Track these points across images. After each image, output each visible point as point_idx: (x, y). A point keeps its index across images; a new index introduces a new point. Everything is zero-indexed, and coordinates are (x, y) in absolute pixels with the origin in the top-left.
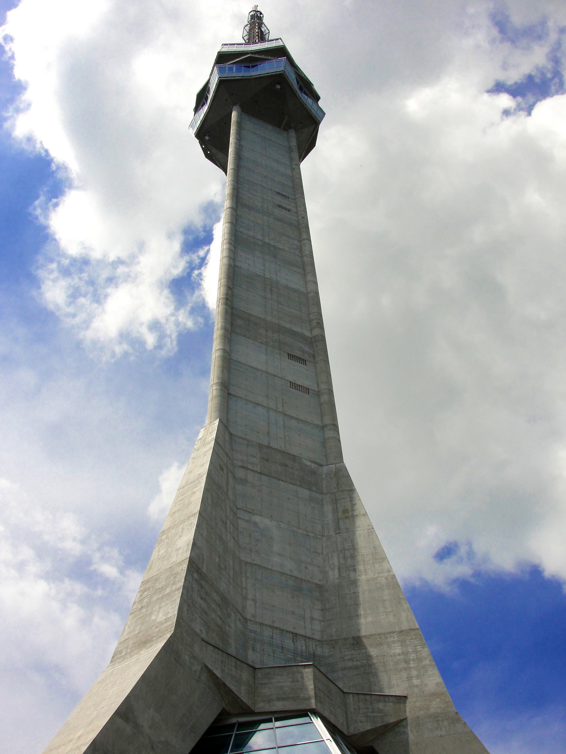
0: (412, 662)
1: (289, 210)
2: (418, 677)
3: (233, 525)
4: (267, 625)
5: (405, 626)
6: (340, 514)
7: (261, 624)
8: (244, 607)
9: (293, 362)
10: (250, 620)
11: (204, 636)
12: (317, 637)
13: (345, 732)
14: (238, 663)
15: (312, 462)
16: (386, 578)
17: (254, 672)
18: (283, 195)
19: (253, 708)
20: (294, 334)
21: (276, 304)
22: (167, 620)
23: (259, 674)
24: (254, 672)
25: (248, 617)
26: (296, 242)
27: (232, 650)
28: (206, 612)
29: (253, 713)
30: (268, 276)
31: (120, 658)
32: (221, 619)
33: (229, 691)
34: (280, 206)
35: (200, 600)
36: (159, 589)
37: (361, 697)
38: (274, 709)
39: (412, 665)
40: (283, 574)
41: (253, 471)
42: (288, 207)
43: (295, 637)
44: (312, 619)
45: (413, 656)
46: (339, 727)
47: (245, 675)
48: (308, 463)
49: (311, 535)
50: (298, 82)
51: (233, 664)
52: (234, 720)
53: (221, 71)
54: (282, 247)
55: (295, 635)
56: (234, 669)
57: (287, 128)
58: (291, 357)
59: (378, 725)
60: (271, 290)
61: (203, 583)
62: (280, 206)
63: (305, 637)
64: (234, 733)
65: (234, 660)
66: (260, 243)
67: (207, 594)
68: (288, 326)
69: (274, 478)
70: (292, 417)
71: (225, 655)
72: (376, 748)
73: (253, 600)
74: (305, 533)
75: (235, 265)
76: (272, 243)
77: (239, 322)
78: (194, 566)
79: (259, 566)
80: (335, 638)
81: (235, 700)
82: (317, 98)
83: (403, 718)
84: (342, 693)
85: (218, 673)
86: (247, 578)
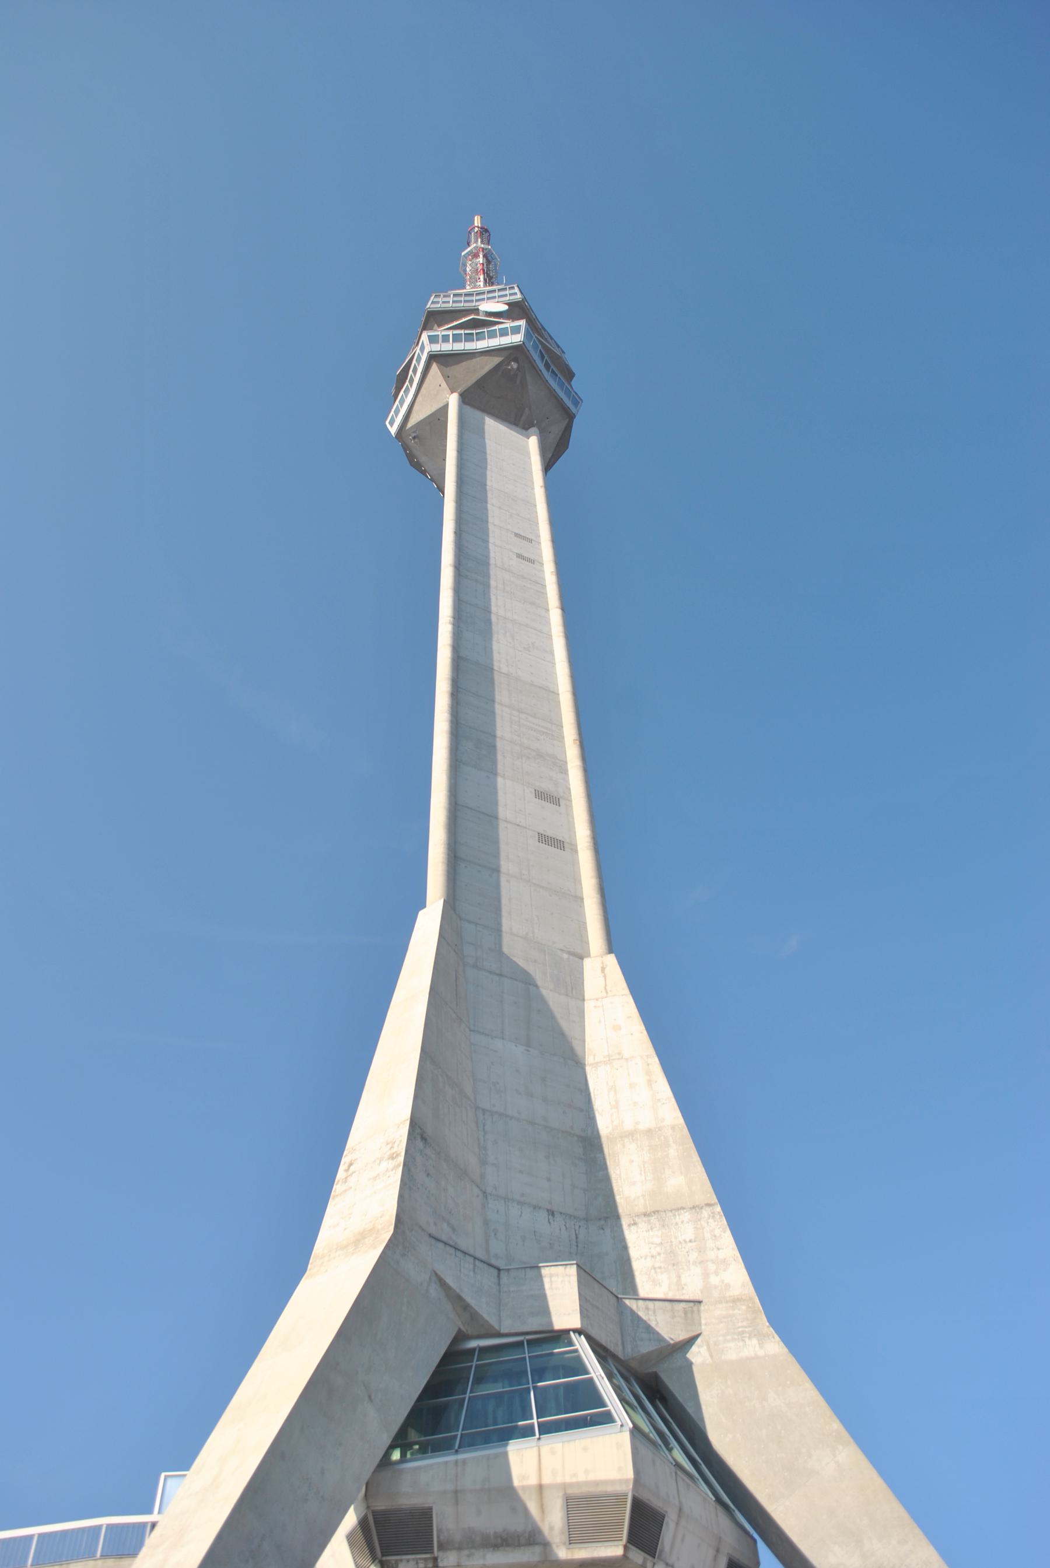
2: (717, 1273)
5: (735, 1292)
8: (482, 1176)
11: (432, 1230)
14: (477, 1262)
17: (499, 1276)
19: (497, 1327)
23: (503, 1274)
24: (499, 1276)
25: (489, 1190)
33: (467, 1307)
46: (612, 1349)
50: (542, 357)
51: (472, 1266)
52: (473, 1344)
56: (472, 1274)
62: (519, 556)
64: (474, 1364)
65: (471, 1259)
70: (486, 1222)
72: (664, 1377)
81: (474, 1316)
82: (569, 375)
83: (695, 1333)
85: (449, 1281)
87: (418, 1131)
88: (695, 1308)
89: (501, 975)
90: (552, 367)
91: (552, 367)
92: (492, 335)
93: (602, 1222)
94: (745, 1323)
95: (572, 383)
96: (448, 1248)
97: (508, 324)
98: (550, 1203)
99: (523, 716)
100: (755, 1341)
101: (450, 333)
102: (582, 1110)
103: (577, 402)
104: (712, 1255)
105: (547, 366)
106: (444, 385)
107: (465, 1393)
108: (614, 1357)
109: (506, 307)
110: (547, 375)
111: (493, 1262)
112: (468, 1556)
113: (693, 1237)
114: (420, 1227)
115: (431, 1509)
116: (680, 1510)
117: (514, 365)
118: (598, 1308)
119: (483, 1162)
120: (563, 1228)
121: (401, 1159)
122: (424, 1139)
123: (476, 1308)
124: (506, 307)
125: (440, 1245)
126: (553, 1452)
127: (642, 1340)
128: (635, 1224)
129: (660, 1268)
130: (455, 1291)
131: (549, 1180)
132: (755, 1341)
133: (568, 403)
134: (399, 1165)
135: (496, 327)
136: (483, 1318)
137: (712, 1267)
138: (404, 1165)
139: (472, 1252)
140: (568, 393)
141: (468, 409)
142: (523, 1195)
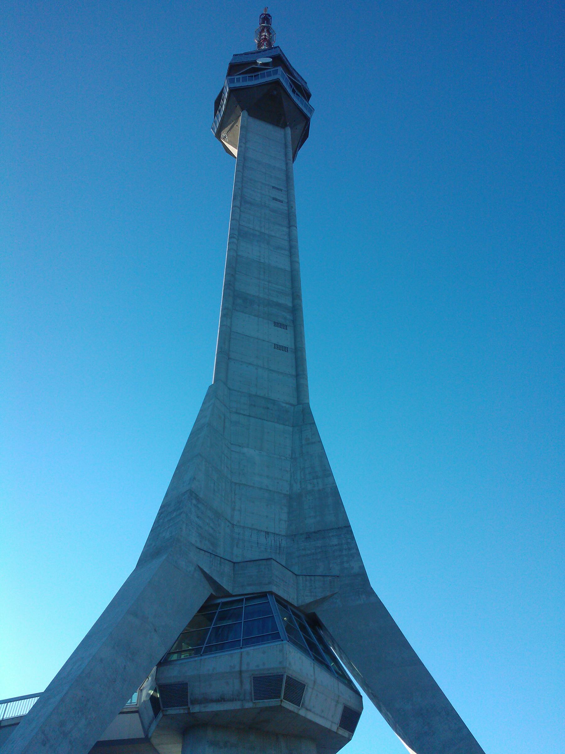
0: (344, 551)
1: (281, 202)
3: (227, 457)
4: (248, 528)
6: (304, 442)
7: (244, 527)
11: (198, 545)
12: (283, 533)
14: (222, 560)
15: (287, 403)
18: (278, 189)
19: (231, 592)
20: (278, 305)
21: (266, 283)
25: (235, 523)
27: (220, 551)
28: (200, 527)
29: (232, 596)
30: (262, 261)
32: (213, 529)
34: (274, 199)
35: (196, 519)
37: (308, 577)
38: (246, 592)
39: (344, 553)
41: (244, 415)
42: (281, 199)
44: (280, 520)
45: (345, 546)
47: (227, 568)
48: (284, 405)
49: (283, 458)
52: (219, 601)
53: (231, 81)
54: (273, 234)
55: (267, 533)
56: (219, 565)
57: (284, 126)
58: (277, 324)
59: (318, 598)
60: (264, 272)
61: (200, 506)
62: (274, 199)
65: (219, 559)
66: (258, 233)
67: (202, 513)
68: (275, 300)
74: (278, 457)
76: (267, 232)
77: (239, 301)
79: (244, 484)
82: (307, 96)
84: (295, 576)
86: (235, 495)
92: (263, 76)
96: (206, 553)
97: (272, 70)
99: (270, 284)
101: (241, 76)
103: (311, 110)
105: (294, 91)
107: (242, 620)
109: (270, 60)
112: (205, 707)
115: (187, 684)
116: (315, 682)
117: (275, 93)
119: (233, 509)
124: (270, 60)
125: (203, 552)
126: (248, 654)
127: (307, 596)
128: (309, 537)
133: (305, 111)
135: (265, 71)
137: (345, 559)
140: (306, 106)
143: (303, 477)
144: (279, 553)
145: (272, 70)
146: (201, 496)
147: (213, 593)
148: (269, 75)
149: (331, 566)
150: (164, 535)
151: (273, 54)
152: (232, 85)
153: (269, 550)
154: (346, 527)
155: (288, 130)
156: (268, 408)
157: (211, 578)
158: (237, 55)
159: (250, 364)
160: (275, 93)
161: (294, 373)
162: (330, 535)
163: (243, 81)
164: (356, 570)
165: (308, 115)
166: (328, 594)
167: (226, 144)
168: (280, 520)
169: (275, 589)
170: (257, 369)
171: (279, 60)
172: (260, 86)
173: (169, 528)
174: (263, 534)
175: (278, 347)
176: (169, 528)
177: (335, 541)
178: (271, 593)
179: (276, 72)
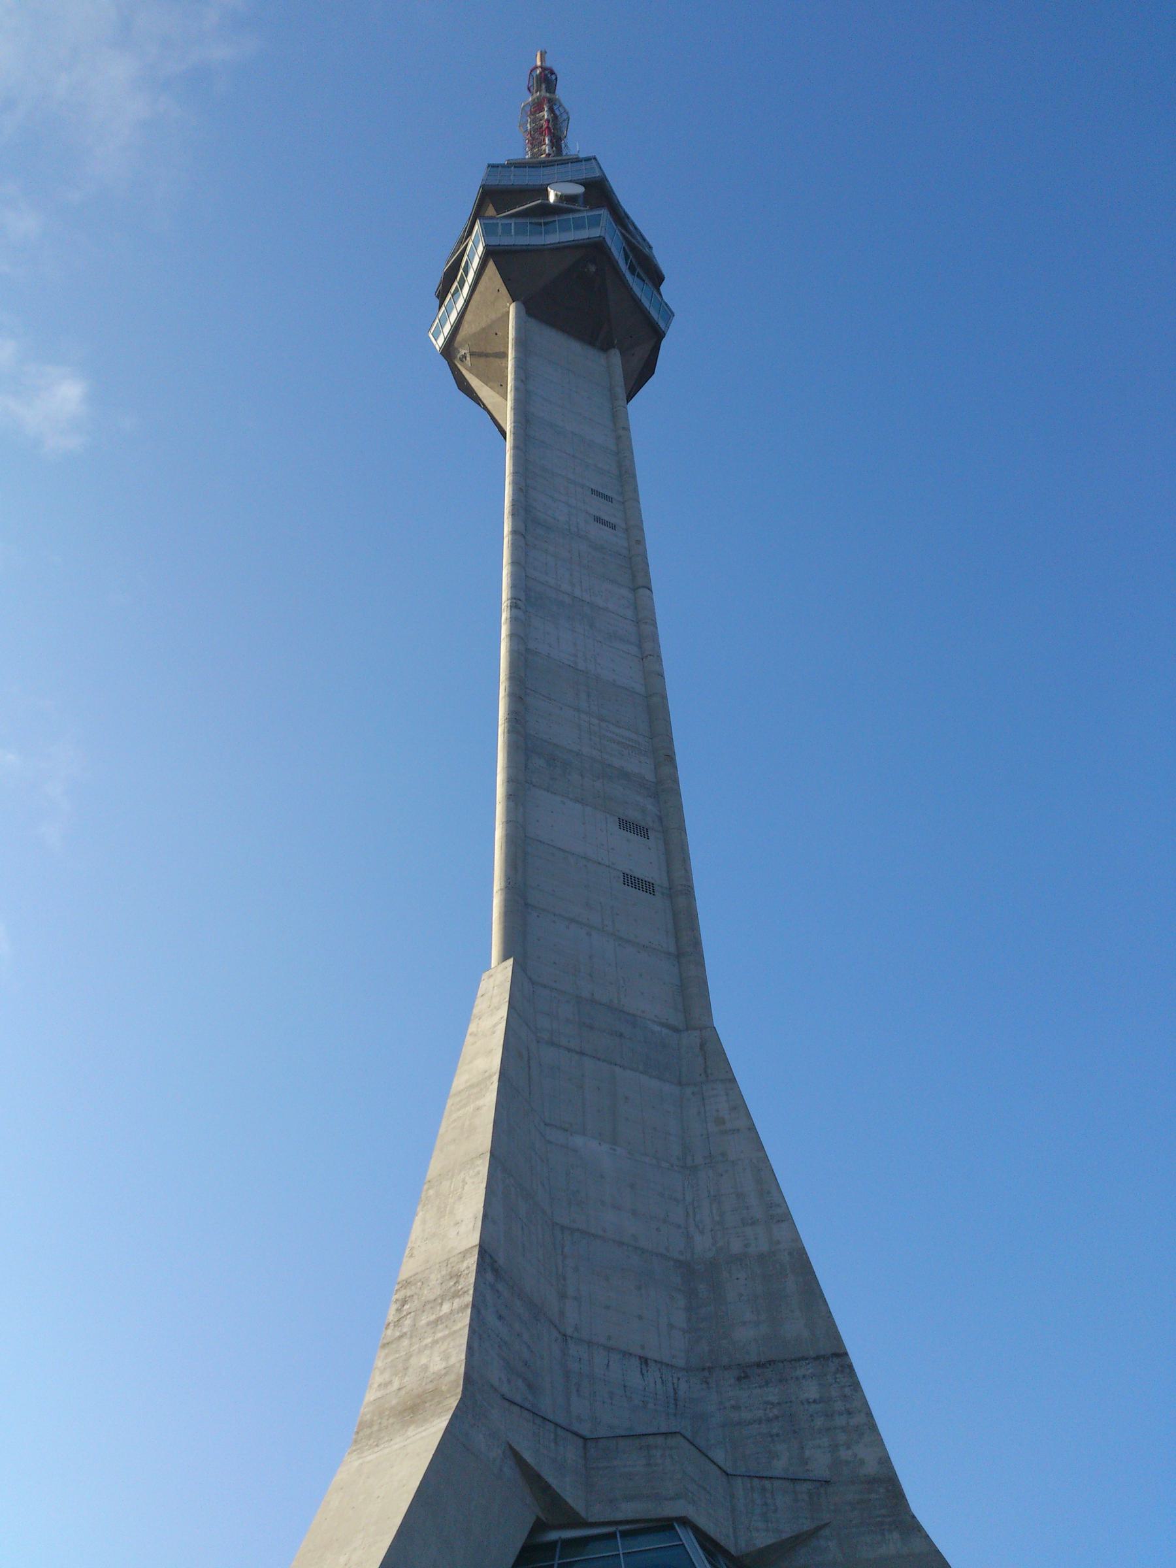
1: (613, 527)
7: (590, 1343)
8: (562, 1313)
9: (631, 836)
10: (572, 1337)
11: (505, 1389)
12: (681, 1363)
13: (732, 1550)
14: (559, 1429)
16: (790, 1254)
19: (583, 1514)
22: (448, 1370)
24: (585, 1447)
25: (569, 1331)
26: (625, 592)
30: (581, 665)
31: (369, 1436)
36: (429, 1302)
37: (756, 1481)
38: (620, 1516)
40: (621, 1244)
41: (569, 1050)
42: (613, 520)
43: (644, 1367)
44: (671, 1326)
47: (571, 1453)
49: (664, 1164)
51: (552, 1436)
52: (553, 1536)
55: (644, 1361)
56: (552, 1445)
57: (605, 348)
59: (784, 1536)
61: (500, 1287)
62: (598, 519)
63: (661, 1363)
65: (551, 1427)
69: (604, 1061)
71: (538, 1421)
73: (576, 1298)
75: (527, 650)
78: (486, 1255)
80: (708, 1365)
82: (656, 278)
85: (527, 1456)
87: (488, 1260)
88: (822, 1491)
89: (582, 1053)
90: (638, 270)
91: (638, 270)
92: (565, 229)
93: (706, 1373)
94: (883, 1511)
95: (662, 288)
96: (525, 1413)
97: (586, 214)
98: (643, 1347)
99: (604, 725)
100: (896, 1535)
101: (513, 221)
102: (679, 1227)
104: (840, 1421)
105: (632, 269)
106: (504, 290)
108: (725, 1552)
109: (580, 190)
110: (629, 277)
111: (575, 1427)
113: (817, 1396)
114: (492, 1386)
117: (593, 269)
118: (705, 1489)
119: (563, 1296)
120: (659, 1381)
121: (469, 1298)
122: (496, 1271)
123: (558, 1491)
124: (580, 190)
125: (516, 1409)
127: (757, 1530)
128: (746, 1377)
129: (778, 1435)
130: (533, 1469)
131: (640, 1318)
132: (896, 1535)
133: (654, 314)
134: (467, 1306)
135: (571, 216)
136: (566, 1503)
137: (842, 1438)
138: (473, 1306)
139: (551, 1417)
141: (533, 325)
142: (609, 1338)
143: (717, 1218)
144: (675, 1415)
145: (585, 214)
146: (501, 1261)
147: (540, 1514)
148: (579, 226)
149: (807, 1453)
150: (424, 1361)
151: (584, 176)
152: (495, 241)
153: (651, 1406)
154: (836, 1355)
155: (616, 357)
156: (621, 1035)
157: (539, 1476)
158: (496, 166)
159: (572, 920)
160: (593, 269)
161: (672, 949)
162: (799, 1373)
163: (517, 233)
164: (871, 1468)
165: (662, 325)
166: (807, 1525)
167: (464, 372)
168: (671, 1326)
169: (689, 1512)
170: (589, 934)
171: (598, 192)
172: (557, 249)
173: (435, 1342)
174: (635, 1362)
175: (631, 881)
176: (435, 1342)
177: (811, 1390)
178: (684, 1522)
179: (595, 222)
